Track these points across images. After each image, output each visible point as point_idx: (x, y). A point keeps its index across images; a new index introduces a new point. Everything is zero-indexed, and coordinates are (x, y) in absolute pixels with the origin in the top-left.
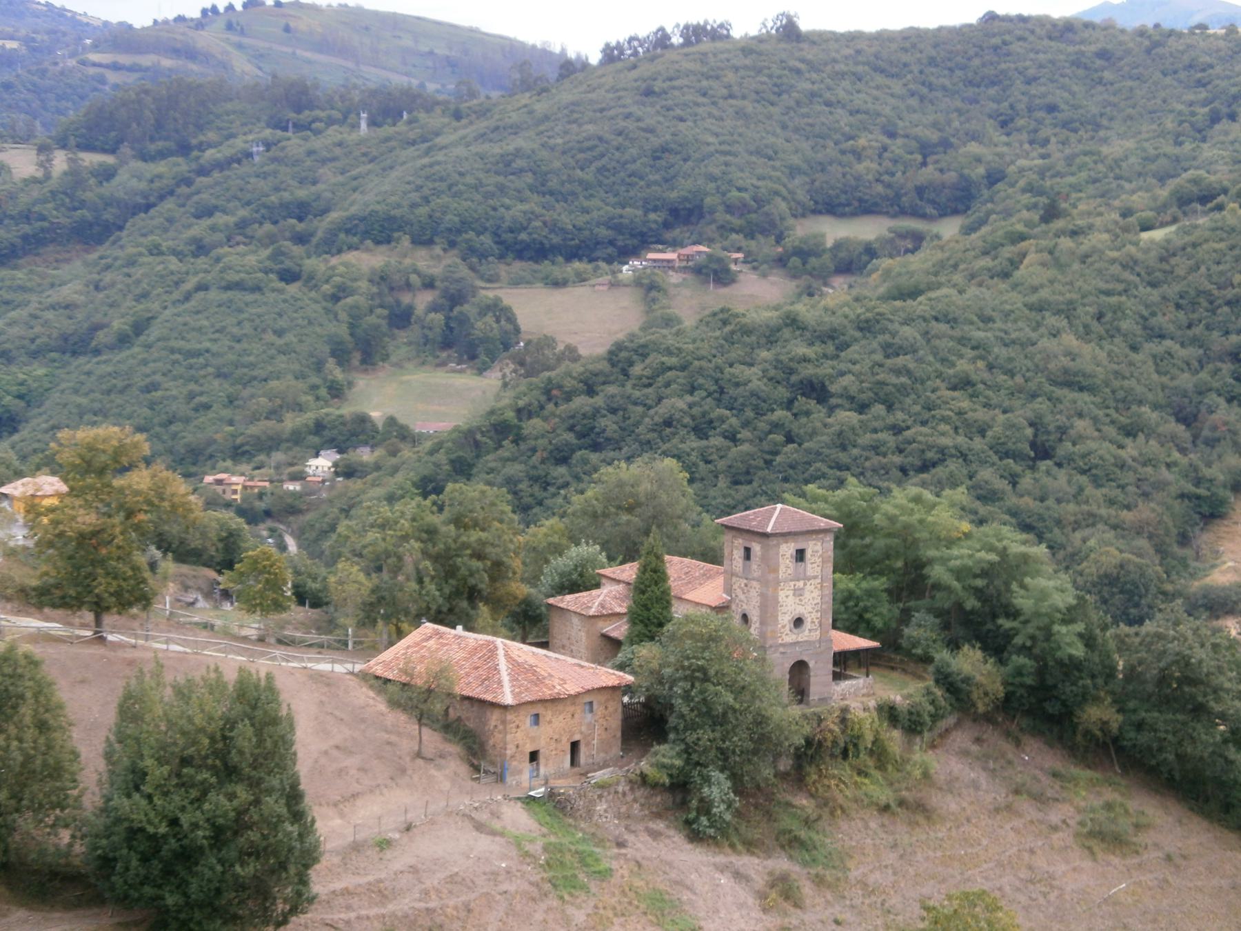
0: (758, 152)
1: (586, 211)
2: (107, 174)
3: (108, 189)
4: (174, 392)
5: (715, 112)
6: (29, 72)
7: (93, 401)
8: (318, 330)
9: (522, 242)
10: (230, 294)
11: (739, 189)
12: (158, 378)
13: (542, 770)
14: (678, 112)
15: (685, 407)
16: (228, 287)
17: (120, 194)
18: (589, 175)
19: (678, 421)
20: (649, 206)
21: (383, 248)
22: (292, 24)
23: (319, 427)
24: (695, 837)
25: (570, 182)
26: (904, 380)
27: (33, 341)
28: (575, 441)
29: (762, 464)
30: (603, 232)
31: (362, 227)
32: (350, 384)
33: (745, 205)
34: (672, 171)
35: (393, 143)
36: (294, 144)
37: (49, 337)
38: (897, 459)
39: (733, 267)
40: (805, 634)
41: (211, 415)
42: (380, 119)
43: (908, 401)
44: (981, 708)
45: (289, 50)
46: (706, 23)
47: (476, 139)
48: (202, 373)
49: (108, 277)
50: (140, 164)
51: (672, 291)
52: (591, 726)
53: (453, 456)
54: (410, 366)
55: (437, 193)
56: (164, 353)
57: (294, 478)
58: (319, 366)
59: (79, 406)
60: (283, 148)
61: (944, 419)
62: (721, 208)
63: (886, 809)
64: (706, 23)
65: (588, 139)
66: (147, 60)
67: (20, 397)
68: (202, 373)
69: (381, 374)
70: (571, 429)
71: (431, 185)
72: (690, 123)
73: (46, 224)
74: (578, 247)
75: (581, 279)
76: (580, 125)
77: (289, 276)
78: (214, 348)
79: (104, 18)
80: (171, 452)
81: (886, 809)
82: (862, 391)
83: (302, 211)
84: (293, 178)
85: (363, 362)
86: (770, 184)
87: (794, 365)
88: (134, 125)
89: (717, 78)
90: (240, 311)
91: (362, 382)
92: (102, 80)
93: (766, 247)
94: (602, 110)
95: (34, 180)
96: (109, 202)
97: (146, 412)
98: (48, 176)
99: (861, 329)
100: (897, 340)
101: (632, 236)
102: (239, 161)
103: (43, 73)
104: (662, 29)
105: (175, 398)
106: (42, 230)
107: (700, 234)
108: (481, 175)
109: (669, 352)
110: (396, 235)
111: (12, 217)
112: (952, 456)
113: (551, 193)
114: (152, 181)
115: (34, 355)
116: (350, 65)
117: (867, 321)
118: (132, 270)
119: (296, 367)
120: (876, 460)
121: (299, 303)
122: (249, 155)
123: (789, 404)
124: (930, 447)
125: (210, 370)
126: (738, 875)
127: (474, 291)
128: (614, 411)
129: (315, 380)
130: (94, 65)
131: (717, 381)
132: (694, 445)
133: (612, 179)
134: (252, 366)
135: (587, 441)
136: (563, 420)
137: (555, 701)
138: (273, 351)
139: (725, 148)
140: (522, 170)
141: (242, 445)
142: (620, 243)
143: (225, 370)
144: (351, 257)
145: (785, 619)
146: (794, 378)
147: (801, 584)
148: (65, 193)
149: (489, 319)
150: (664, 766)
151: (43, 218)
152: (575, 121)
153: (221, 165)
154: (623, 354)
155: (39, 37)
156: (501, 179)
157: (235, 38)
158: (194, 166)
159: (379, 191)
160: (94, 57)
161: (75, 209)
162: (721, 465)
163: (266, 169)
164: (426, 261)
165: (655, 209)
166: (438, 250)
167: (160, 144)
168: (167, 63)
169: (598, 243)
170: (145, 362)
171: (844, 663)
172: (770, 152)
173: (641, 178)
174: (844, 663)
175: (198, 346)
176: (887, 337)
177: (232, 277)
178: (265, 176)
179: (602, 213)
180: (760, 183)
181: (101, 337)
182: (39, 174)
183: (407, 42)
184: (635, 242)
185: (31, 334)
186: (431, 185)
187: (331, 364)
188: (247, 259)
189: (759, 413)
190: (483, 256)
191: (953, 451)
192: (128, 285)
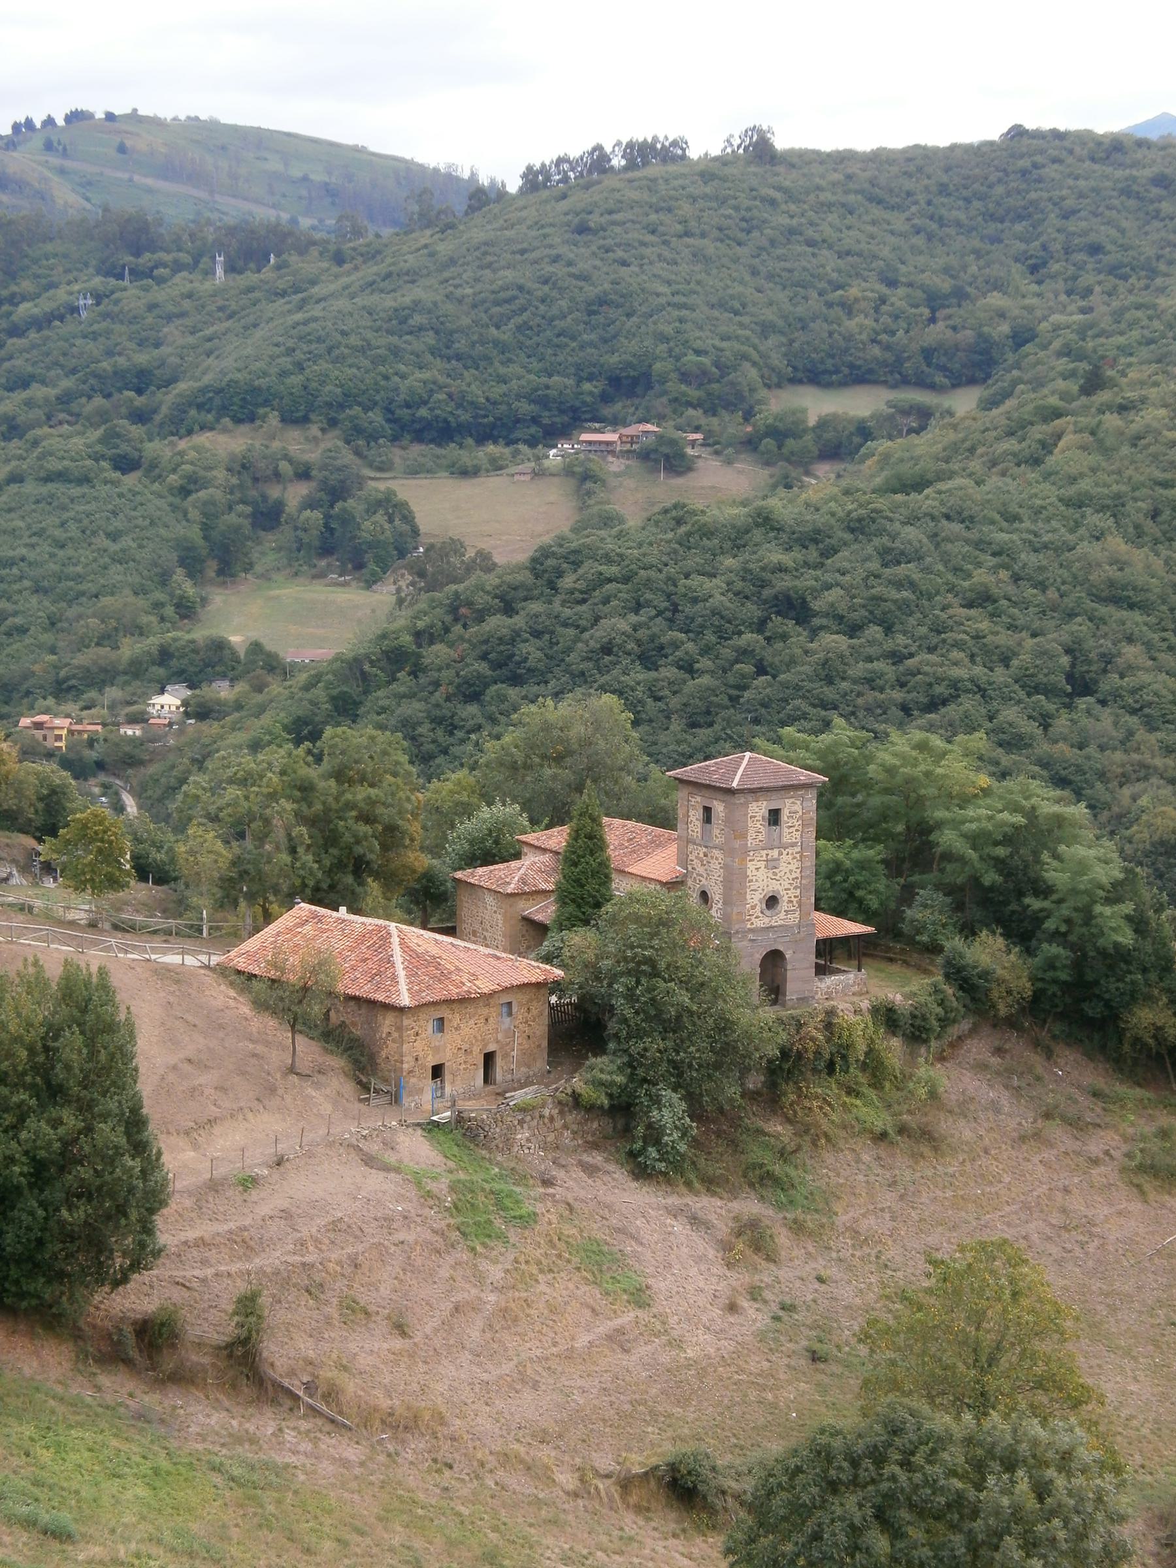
0: (722, 305)
1: (503, 380)
8: (162, 531)
9: (422, 419)
10: (51, 486)
11: (698, 352)
13: (448, 1089)
14: (620, 253)
15: (628, 629)
16: (48, 479)
18: (505, 335)
19: (620, 647)
20: (583, 373)
21: (244, 428)
22: (129, 143)
24: (642, 1173)
30: (525, 408)
31: (217, 401)
32: (204, 601)
33: (704, 373)
34: (612, 329)
35: (257, 294)
36: (132, 296)
38: (898, 695)
39: (689, 451)
40: (779, 918)
41: (28, 640)
45: (126, 176)
48: (16, 587)
51: (612, 482)
52: (510, 1034)
53: (335, 692)
54: (278, 577)
55: (315, 358)
57: (133, 720)
58: (164, 579)
60: (117, 302)
61: (957, 645)
62: (673, 375)
63: (882, 1137)
65: (505, 288)
68: (16, 587)
70: (484, 657)
72: (634, 268)
74: (493, 426)
75: (496, 466)
76: (494, 271)
77: (125, 464)
78: (31, 555)
81: (882, 1137)
83: (142, 380)
84: (130, 339)
85: (220, 572)
86: (737, 346)
87: (767, 576)
89: (669, 210)
90: (64, 508)
91: (218, 598)
93: (732, 426)
94: (523, 252)
100: (897, 544)
101: (562, 412)
104: (599, 148)
108: (369, 335)
109: (608, 559)
110: (261, 411)
112: (968, 691)
113: (458, 357)
116: (203, 195)
120: (871, 696)
121: (138, 498)
122: (74, 310)
123: (760, 626)
124: (939, 680)
125: (27, 583)
126: (695, 1221)
127: (361, 481)
128: (537, 634)
129: (159, 595)
131: (669, 596)
132: (640, 677)
134: (78, 578)
136: (474, 646)
137: (464, 1001)
142: (546, 421)
144: (203, 439)
145: (755, 899)
146: (767, 593)
147: (775, 853)
149: (380, 517)
150: (602, 1084)
154: (551, 562)
156: (394, 339)
157: (55, 161)
159: (236, 357)
162: (675, 702)
163: (96, 327)
164: (302, 445)
165: (590, 379)
166: (314, 430)
169: (518, 421)
171: (830, 953)
172: (737, 305)
173: (573, 338)
174: (830, 953)
175: (11, 553)
176: (885, 540)
177: (54, 465)
178: (95, 336)
179: (523, 382)
180: (725, 344)
183: (274, 165)
187: (179, 575)
188: (72, 443)
190: (372, 437)
191: (969, 685)
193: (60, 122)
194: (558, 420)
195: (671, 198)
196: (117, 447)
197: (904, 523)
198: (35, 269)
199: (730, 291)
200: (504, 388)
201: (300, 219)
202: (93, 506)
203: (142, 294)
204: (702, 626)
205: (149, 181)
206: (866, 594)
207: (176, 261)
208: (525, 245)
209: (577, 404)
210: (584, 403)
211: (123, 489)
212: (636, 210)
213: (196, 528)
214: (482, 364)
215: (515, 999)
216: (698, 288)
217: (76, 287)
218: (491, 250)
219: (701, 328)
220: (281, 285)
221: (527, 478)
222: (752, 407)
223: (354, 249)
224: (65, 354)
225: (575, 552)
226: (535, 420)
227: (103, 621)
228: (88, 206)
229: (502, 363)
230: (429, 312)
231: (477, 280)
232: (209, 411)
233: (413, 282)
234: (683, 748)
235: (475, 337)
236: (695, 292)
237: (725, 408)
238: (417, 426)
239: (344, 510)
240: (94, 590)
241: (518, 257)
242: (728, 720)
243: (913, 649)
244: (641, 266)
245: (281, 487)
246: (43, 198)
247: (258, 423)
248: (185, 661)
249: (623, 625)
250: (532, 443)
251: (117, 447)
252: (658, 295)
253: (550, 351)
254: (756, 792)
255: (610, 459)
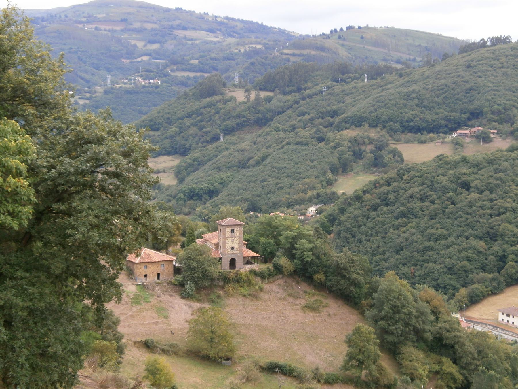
0: (509, 90)
1: (437, 114)
2: (269, 100)
3: (268, 106)
4: (271, 183)
5: (495, 74)
6: (261, 58)
7: (243, 185)
8: (326, 160)
9: (411, 126)
10: (297, 146)
11: (498, 105)
12: (267, 177)
13: (148, 279)
14: (479, 74)
15: (418, 191)
16: (297, 144)
17: (273, 108)
18: (439, 100)
19: (415, 196)
20: (463, 112)
21: (358, 129)
22: (364, 36)
23: (318, 196)
24: (183, 297)
25: (432, 102)
26: (498, 182)
27: (229, 163)
28: (380, 203)
29: (441, 212)
30: (443, 122)
31: (351, 121)
32: (336, 180)
33: (500, 111)
34: (473, 98)
35: (375, 87)
36: (338, 88)
37: (235, 162)
38: (489, 211)
39: (492, 136)
40: (234, 252)
41: (283, 191)
42: (375, 77)
43: (499, 190)
44: (286, 273)
45: (362, 46)
46: (501, 36)
47: (400, 86)
48: (282, 175)
49: (259, 139)
50: (282, 96)
51: (466, 145)
52: (163, 270)
53: (340, 207)
54: (361, 173)
55: (380, 107)
56: (270, 168)
57: (302, 214)
58: (324, 174)
59: (238, 187)
60: (333, 89)
61: (510, 197)
62: (489, 112)
63: (245, 296)
64: (501, 36)
65: (441, 86)
66: (305, 52)
67: (221, 183)
68: (282, 175)
69: (349, 177)
70: (379, 198)
71: (378, 104)
72: (483, 79)
73: (245, 119)
74: (433, 128)
75: (432, 140)
76: (440, 80)
77: (321, 140)
78: (288, 166)
79: (300, 33)
80: (267, 204)
81: (245, 296)
82: (482, 186)
83: (334, 114)
84: (336, 101)
85: (343, 172)
86: (511, 102)
87: (460, 176)
88: (281, 81)
89: (498, 60)
90: (300, 153)
91: (341, 179)
92: (288, 60)
93: (507, 128)
94: (449, 74)
95: (244, 103)
96: (269, 111)
97: (261, 189)
98: (248, 101)
99: (489, 163)
100: (500, 167)
101: (455, 123)
102: (317, 95)
103: (266, 58)
104: (483, 39)
105: (271, 185)
106: (244, 121)
107: (481, 123)
108: (398, 100)
109: (418, 171)
110: (363, 123)
111: (233, 117)
112: (509, 211)
113: (424, 107)
114: (285, 102)
115: (228, 168)
116: (386, 51)
117: (491, 160)
118: (267, 137)
119: (316, 173)
120: (482, 211)
121: (321, 150)
122: (322, 92)
123: (455, 191)
124: (502, 207)
126: (190, 306)
127: (387, 145)
128: (394, 192)
129: (323, 179)
130: (286, 54)
131: (432, 181)
132: (419, 205)
133: (449, 101)
134: (300, 173)
135: (384, 203)
136: (377, 195)
137: (151, 263)
138: (309, 168)
139: (495, 88)
140: (414, 98)
141: (291, 203)
142: (449, 126)
143: (291, 175)
144: (345, 132)
145: (228, 247)
146: (459, 181)
147: (233, 238)
148: (253, 107)
149: (391, 156)
150: (178, 280)
151: (244, 117)
152: (438, 78)
153: (310, 96)
154: (402, 171)
155: (270, 43)
156: (405, 101)
157: (341, 42)
158: (301, 97)
159: (361, 106)
160: (286, 51)
161: (256, 113)
162: (427, 212)
163: (326, 97)
164: (373, 134)
165: (465, 113)
166: (378, 129)
167: (291, 88)
168: (313, 53)
169: (441, 126)
170: (263, 171)
171: (248, 261)
172: (514, 90)
173: (460, 101)
174: (248, 261)
175: (283, 166)
176: (497, 166)
177: (299, 140)
179: (443, 114)
180: (508, 102)
181: (251, 162)
182: (245, 100)
183: (410, 41)
184: (456, 125)
185: (228, 160)
186: (378, 104)
187: (329, 173)
188: (306, 133)
189: (444, 193)
190: (395, 131)
191: (510, 209)
192: (265, 143)
193: (345, 29)
194: (453, 126)
195: (499, 56)
196: (319, 134)
197: (504, 161)
198: (313, 80)
199: (513, 85)
200: (437, 116)
201: (417, 58)
202: (306, 152)
203: (341, 87)
204: (439, 190)
205: (370, 48)
206: (487, 181)
207: (354, 76)
208: (450, 72)
209: (460, 121)
210: (462, 121)
211: (317, 147)
212: (487, 60)
213: (336, 159)
214: (432, 109)
215: (165, 263)
216: (502, 85)
217: (323, 85)
218: (440, 73)
219: (501, 97)
220: (382, 84)
221: (440, 144)
222: (514, 122)
223: (406, 73)
224: (316, 106)
225: (409, 168)
226: (446, 126)
227: (304, 186)
228: (350, 56)
229: (438, 109)
230: (417, 93)
231: (434, 83)
232: (348, 124)
233: (415, 83)
234: (427, 225)
235: (430, 101)
236: (501, 86)
237: (505, 122)
238: (410, 128)
239: (380, 154)
240: (304, 177)
241: (448, 75)
242: (440, 218)
243: (497, 198)
244: (485, 78)
245: (365, 146)
246: (336, 54)
247: (362, 127)
248: (323, 198)
249: (417, 190)
250: (446, 133)
251: (319, 134)
252: (488, 87)
253: (453, 105)
254: (228, 226)
255: (466, 138)
